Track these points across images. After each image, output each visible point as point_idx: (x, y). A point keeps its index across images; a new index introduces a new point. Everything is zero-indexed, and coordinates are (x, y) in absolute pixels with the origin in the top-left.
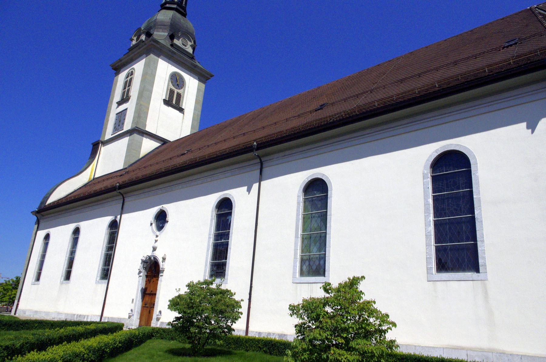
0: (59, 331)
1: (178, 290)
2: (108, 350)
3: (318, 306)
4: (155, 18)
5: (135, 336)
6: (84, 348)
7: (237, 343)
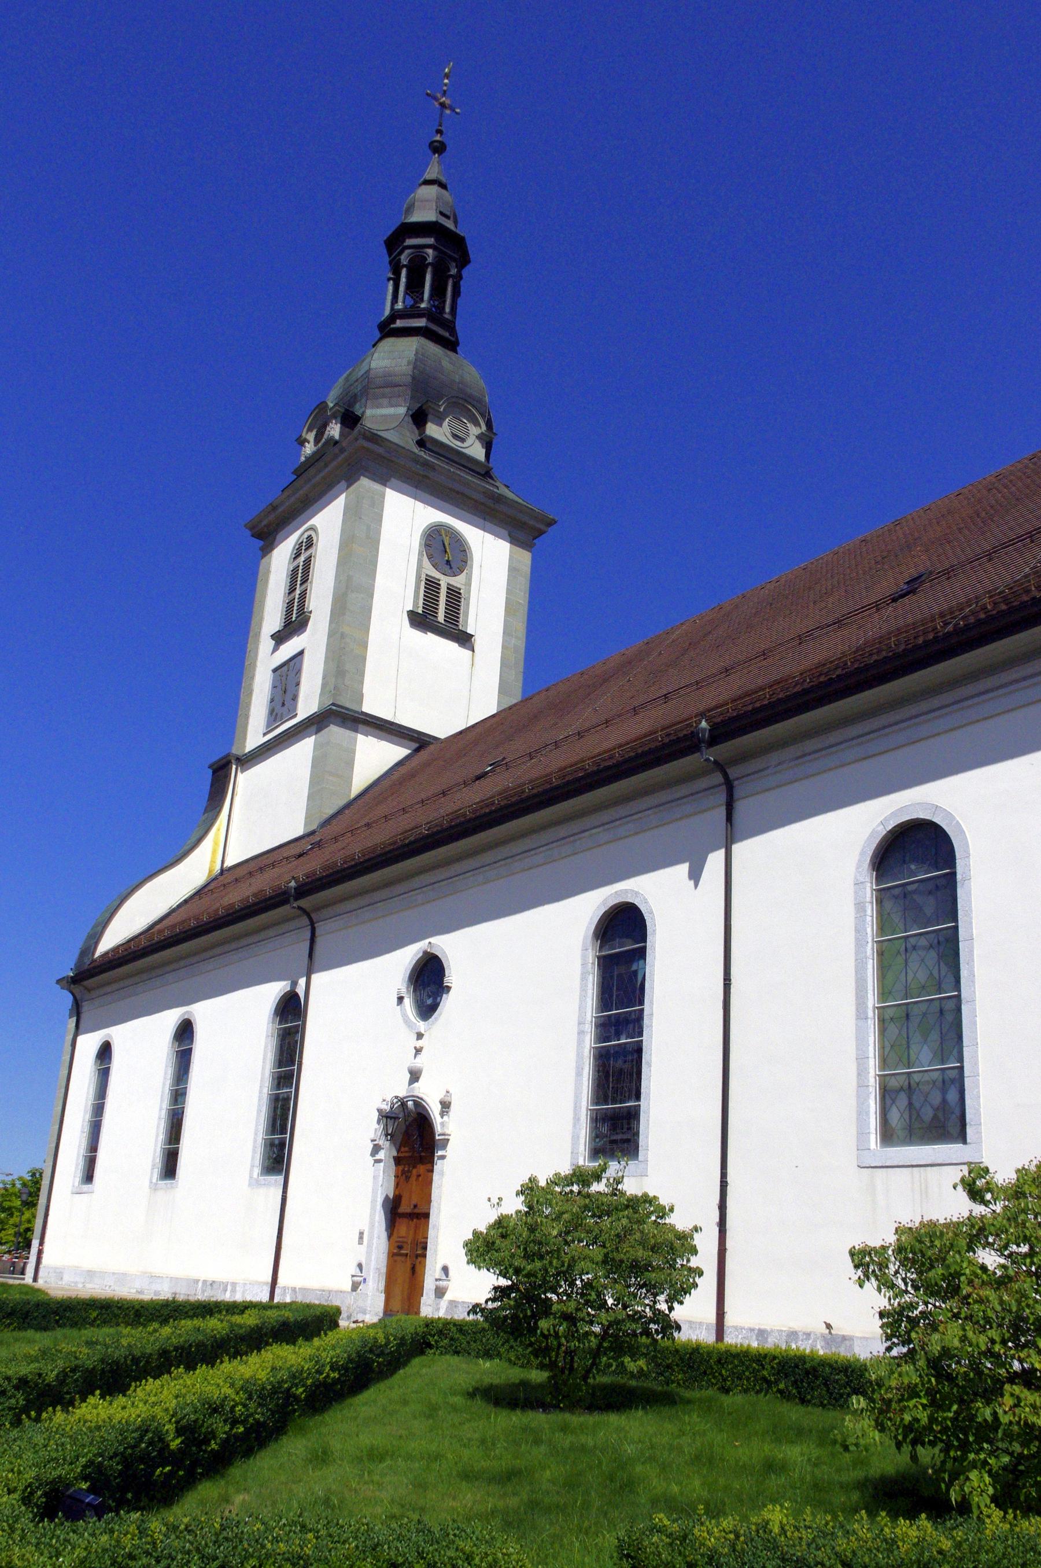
0: (157, 1334)
1: (495, 1201)
2: (301, 1390)
3: (952, 1245)
4: (364, 367)
5: (375, 1348)
6: (232, 1385)
7: (693, 1367)
